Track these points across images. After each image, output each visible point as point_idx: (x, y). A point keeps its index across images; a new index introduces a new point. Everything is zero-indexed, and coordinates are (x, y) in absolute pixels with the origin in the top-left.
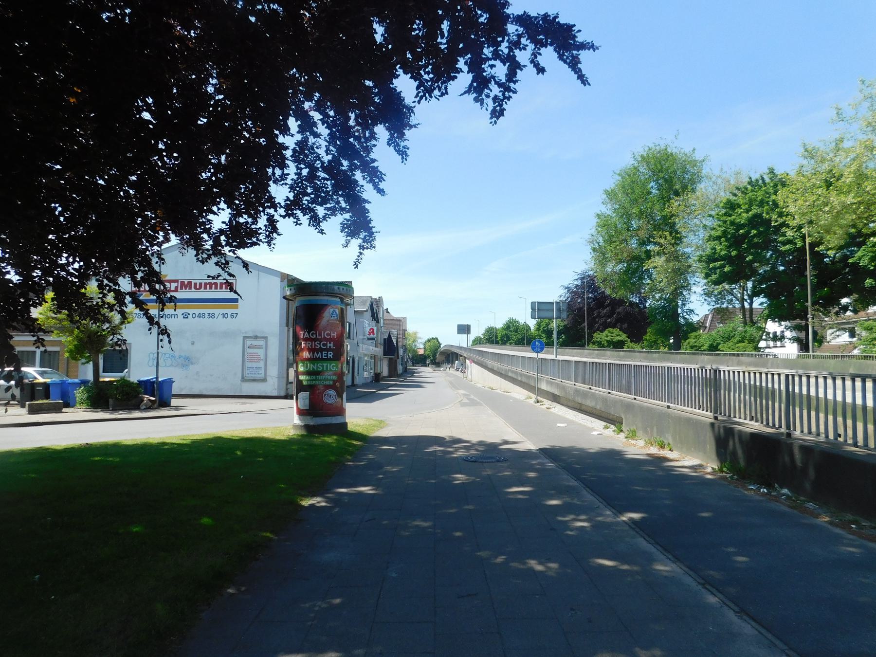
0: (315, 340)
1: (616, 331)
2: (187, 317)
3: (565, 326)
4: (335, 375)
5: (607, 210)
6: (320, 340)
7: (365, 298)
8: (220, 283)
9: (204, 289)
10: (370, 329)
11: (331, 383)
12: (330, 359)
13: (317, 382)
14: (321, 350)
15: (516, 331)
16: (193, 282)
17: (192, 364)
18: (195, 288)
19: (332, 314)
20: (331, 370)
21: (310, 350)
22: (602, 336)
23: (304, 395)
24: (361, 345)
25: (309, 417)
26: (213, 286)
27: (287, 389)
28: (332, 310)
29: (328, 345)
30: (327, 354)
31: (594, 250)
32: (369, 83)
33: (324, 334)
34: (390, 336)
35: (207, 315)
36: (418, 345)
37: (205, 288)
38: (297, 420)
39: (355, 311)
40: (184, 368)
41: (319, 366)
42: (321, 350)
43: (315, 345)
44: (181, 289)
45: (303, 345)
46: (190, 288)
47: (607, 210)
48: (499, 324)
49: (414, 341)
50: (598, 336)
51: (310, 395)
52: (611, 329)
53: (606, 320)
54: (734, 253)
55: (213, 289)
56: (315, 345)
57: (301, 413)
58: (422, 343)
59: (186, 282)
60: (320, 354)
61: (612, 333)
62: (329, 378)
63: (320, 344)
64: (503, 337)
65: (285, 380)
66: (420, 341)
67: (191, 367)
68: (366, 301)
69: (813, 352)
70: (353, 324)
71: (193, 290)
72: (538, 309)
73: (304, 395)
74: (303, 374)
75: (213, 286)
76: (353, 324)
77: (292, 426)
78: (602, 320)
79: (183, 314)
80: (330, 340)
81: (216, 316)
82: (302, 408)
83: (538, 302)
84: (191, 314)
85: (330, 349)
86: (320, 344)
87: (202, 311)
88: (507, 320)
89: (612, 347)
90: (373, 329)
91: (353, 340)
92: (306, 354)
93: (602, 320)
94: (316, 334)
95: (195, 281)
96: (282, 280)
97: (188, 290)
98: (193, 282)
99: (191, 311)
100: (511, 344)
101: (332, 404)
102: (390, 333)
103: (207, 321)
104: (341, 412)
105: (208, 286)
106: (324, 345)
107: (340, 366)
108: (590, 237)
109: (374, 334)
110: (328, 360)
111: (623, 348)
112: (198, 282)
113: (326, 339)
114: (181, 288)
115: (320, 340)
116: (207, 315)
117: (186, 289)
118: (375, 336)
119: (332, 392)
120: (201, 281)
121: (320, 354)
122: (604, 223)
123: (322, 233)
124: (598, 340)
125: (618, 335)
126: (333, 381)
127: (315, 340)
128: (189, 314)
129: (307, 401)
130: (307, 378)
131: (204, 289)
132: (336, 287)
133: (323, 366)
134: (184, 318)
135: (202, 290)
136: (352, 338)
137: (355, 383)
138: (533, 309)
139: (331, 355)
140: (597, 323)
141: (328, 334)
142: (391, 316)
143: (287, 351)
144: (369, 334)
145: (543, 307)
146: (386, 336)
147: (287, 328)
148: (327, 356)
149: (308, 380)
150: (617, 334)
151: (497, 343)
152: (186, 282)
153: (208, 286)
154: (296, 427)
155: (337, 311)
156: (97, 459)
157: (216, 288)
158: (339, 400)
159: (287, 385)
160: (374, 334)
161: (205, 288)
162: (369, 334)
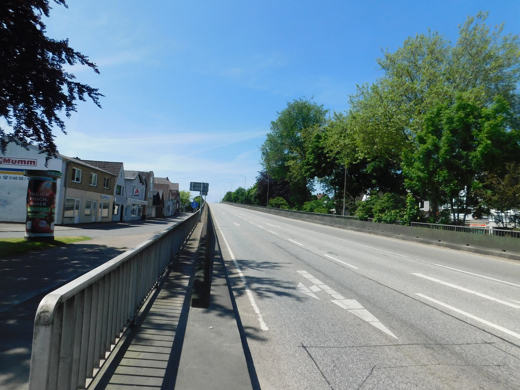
0: (37, 197)
1: (281, 198)
2: (7, 179)
3: (258, 194)
4: (46, 213)
5: (270, 131)
6: (39, 197)
7: (135, 172)
8: (28, 161)
9: (18, 164)
10: (136, 190)
11: (44, 217)
12: (44, 206)
13: (35, 217)
14: (39, 202)
15: (242, 195)
16: (11, 159)
17: (8, 204)
18: (12, 162)
19: (47, 185)
20: (44, 211)
21: (34, 201)
22: (273, 201)
23: (29, 222)
24: (129, 199)
25: (31, 233)
26: (23, 162)
27: (63, 221)
28: (47, 183)
29: (44, 199)
30: (43, 204)
31: (263, 153)
32: (31, 96)
33: (42, 194)
34: (158, 194)
35: (18, 178)
36: (190, 200)
37: (18, 163)
38: (26, 235)
39: (125, 179)
40: (3, 207)
41: (38, 209)
42: (39, 202)
43: (36, 199)
44: (3, 163)
45: (31, 199)
46: (9, 163)
47: (270, 131)
48: (233, 190)
49: (188, 197)
50: (271, 201)
51: (32, 223)
52: (278, 197)
53: (279, 192)
54: (316, 162)
55: (29, 165)
56: (36, 199)
57: (28, 231)
58: (192, 199)
59: (7, 159)
60: (38, 203)
61: (279, 199)
62: (43, 215)
63: (39, 199)
64: (234, 198)
65: (62, 216)
66: (191, 197)
67: (7, 206)
68: (136, 173)
69: (345, 215)
70: (123, 187)
71: (11, 163)
72: (194, 186)
73: (29, 222)
74: (30, 212)
75: (23, 162)
76: (123, 187)
77: (23, 237)
78: (278, 192)
79: (4, 177)
80: (45, 197)
81: (24, 179)
82: (28, 229)
83: (194, 182)
84: (9, 177)
85: (44, 201)
86: (39, 199)
87: (15, 176)
88: (238, 188)
89: (277, 207)
90: (138, 190)
91: (123, 195)
92: (31, 203)
93: (278, 192)
94: (37, 194)
95: (13, 159)
96: (63, 162)
97: (7, 164)
98: (11, 159)
99: (9, 175)
100: (239, 202)
101: (43, 227)
102: (158, 192)
103: (18, 181)
104: (52, 231)
105: (20, 162)
106: (41, 199)
107: (50, 209)
108: (262, 146)
109: (138, 193)
110: (43, 206)
111: (280, 208)
112: (14, 159)
113: (43, 197)
114: (4, 162)
115: (39, 197)
116: (18, 178)
117: (6, 163)
118: (139, 194)
119: (44, 222)
120: (16, 159)
121: (38, 203)
122: (271, 140)
123: (28, 150)
124: (271, 203)
125: (281, 201)
126: (45, 216)
127: (37, 197)
128: (8, 177)
129: (31, 225)
130: (32, 214)
131: (18, 164)
132: (49, 173)
133: (40, 209)
134: (4, 179)
135: (17, 164)
136: (122, 194)
137: (123, 219)
138: (191, 185)
139: (44, 204)
140: (275, 193)
141: (43, 194)
142: (170, 182)
143: (64, 199)
144: (136, 193)
145: (196, 185)
146: (155, 194)
147: (64, 188)
148: (43, 205)
149: (31, 215)
150: (281, 200)
151: (232, 201)
152: (7, 159)
153: (20, 162)
154: (25, 237)
155: (50, 184)
156: (46, 279)
157: (25, 163)
158: (48, 225)
159: (63, 219)
160: (138, 193)
161: (18, 163)
162: (136, 193)
